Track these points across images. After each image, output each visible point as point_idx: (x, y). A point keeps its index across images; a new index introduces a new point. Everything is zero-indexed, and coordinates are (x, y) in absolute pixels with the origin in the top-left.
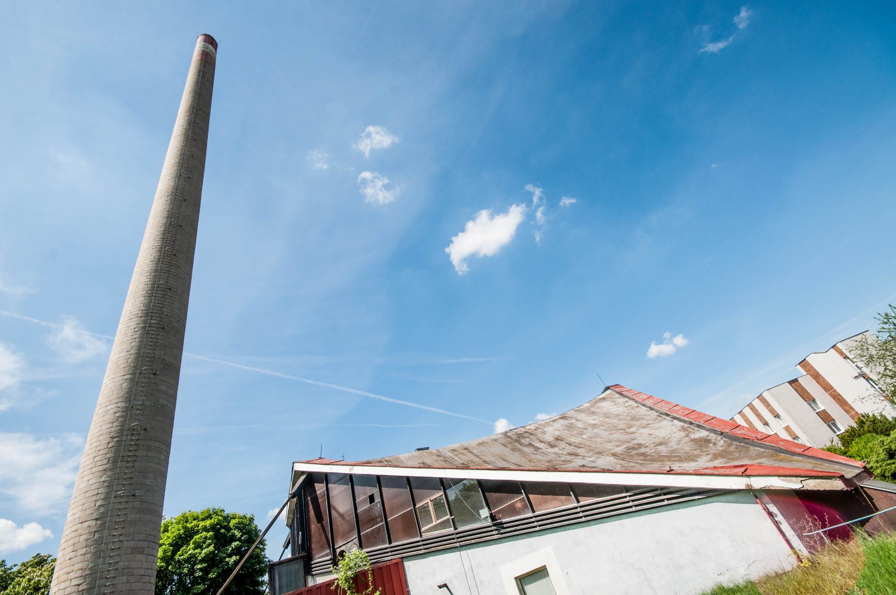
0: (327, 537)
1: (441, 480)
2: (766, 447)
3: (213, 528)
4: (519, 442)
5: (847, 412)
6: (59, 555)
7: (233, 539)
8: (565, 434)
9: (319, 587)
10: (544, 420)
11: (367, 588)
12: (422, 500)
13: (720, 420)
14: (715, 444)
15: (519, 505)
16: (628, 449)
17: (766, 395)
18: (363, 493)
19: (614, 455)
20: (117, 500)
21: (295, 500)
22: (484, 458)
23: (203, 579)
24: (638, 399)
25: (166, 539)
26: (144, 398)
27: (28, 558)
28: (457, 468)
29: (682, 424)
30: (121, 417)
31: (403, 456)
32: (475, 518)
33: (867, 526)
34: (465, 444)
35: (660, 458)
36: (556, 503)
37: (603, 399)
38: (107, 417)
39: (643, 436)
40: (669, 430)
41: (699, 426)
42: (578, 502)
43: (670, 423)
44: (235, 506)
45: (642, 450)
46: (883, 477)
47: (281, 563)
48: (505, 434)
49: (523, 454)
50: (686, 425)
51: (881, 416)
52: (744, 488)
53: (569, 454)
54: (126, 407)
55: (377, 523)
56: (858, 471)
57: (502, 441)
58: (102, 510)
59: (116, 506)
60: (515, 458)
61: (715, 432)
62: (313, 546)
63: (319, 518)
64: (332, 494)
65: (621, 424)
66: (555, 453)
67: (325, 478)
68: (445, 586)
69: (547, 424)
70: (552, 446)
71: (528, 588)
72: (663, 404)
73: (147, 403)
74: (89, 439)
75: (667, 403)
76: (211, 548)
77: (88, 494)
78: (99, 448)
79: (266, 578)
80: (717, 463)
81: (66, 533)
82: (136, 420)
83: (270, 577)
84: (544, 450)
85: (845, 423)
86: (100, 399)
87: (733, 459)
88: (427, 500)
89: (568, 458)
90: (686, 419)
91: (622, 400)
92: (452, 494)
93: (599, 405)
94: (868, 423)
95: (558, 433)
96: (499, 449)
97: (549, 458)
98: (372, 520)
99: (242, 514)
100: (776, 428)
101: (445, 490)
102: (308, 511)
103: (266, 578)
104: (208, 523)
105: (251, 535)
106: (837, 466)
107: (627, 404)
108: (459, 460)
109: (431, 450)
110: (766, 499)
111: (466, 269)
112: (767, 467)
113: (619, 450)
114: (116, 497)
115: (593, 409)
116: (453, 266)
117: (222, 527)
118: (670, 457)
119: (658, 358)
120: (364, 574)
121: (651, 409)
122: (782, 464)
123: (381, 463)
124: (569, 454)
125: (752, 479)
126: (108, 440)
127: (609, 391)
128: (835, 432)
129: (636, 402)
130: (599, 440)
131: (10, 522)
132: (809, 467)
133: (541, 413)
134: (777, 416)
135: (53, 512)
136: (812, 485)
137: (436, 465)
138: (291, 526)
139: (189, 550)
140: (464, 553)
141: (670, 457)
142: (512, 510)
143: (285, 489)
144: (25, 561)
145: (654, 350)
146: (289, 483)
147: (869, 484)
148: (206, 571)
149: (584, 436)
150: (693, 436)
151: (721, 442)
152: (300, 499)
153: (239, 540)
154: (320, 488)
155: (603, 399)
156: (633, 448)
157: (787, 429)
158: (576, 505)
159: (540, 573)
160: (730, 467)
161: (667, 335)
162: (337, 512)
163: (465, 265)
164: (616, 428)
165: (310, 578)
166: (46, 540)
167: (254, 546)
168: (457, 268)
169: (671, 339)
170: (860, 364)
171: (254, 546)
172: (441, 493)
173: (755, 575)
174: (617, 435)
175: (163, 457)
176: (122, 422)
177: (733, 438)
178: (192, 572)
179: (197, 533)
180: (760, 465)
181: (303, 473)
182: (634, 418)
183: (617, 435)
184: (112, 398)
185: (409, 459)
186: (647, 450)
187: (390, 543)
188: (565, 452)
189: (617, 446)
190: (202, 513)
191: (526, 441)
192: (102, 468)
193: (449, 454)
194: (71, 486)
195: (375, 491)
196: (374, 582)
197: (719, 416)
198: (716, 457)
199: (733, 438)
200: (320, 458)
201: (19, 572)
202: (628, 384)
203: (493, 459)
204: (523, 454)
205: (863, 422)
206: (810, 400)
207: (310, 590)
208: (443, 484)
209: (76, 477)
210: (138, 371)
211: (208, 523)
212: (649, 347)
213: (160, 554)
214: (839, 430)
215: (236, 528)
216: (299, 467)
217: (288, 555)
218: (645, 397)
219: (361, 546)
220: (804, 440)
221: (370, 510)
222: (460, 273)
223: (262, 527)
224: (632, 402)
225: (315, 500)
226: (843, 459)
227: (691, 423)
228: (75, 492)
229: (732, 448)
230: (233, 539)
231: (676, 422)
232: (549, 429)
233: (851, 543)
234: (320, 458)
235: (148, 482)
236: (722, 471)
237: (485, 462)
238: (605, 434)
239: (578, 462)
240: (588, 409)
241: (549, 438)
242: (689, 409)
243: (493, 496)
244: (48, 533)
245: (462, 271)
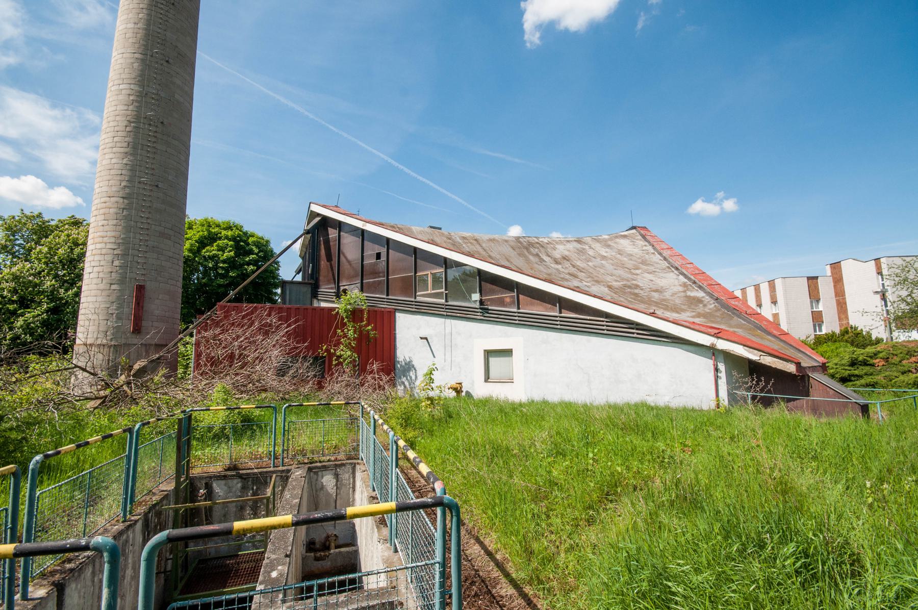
0: (333, 275)
1: (445, 259)
2: (749, 322)
3: (233, 239)
4: (527, 249)
5: (840, 319)
6: (92, 220)
7: (251, 252)
8: (573, 256)
9: (323, 309)
10: (558, 239)
11: (362, 321)
12: (423, 271)
13: (724, 289)
14: (705, 306)
15: (508, 300)
16: (625, 286)
17: (779, 284)
18: (371, 249)
19: (610, 287)
20: (142, 186)
21: (309, 236)
22: (491, 254)
23: (223, 276)
24: (658, 247)
25: (193, 235)
26: (158, 87)
27: (65, 217)
28: (463, 253)
29: (686, 280)
30: (137, 101)
31: (415, 229)
32: (468, 299)
33: (790, 404)
34: (477, 235)
35: (649, 302)
36: (541, 308)
37: (625, 236)
38: (121, 97)
39: (644, 280)
40: (671, 282)
41: (700, 287)
42: (560, 312)
43: (675, 277)
44: (256, 225)
45: (636, 291)
46: (832, 376)
47: (292, 283)
48: (517, 239)
49: (528, 261)
50: (689, 283)
51: (868, 333)
52: (708, 345)
53: (569, 274)
54: (140, 92)
55: (379, 277)
56: (816, 364)
57: (512, 244)
58: (127, 190)
59: (141, 191)
60: (520, 262)
61: (711, 296)
62: (321, 278)
63: (329, 258)
64: (343, 241)
65: (630, 264)
66: (557, 269)
67: (339, 225)
68: (426, 339)
69: (560, 242)
70: (557, 262)
71: (492, 360)
72: (679, 258)
73: (163, 94)
74: (105, 116)
75: (683, 258)
76: (232, 254)
77: (112, 172)
78: (116, 129)
79: (279, 291)
80: (697, 320)
81: (96, 202)
82: (152, 110)
83: (282, 290)
84: (548, 264)
85: (830, 326)
86: (111, 74)
87: (713, 322)
88: (429, 272)
89: (568, 277)
90: (692, 277)
91: (643, 243)
92: (453, 273)
93: (617, 240)
94: (850, 335)
95: (567, 253)
96: (507, 250)
97: (550, 271)
98: (375, 273)
99: (260, 235)
100: (767, 311)
101: (446, 268)
102: (320, 250)
103: (279, 291)
104: (230, 233)
105: (266, 254)
106: (800, 355)
107: (645, 248)
108: (466, 248)
109: (443, 231)
110: (721, 358)
111: (537, 41)
112: (739, 336)
113: (615, 284)
114: (140, 182)
115: (609, 243)
116: (521, 31)
117: (241, 240)
118: (657, 304)
119: (698, 216)
120: (362, 311)
121: (665, 259)
122: (754, 339)
123: (393, 228)
124: (569, 274)
125: (720, 341)
126: (125, 123)
127: (634, 231)
128: (815, 331)
129: (654, 248)
130: (602, 271)
131: (39, 181)
132: (776, 347)
133: (556, 231)
134: (774, 302)
135: (81, 183)
136: (768, 361)
137: (445, 245)
138: (303, 257)
139: (210, 250)
140: (448, 321)
141: (657, 304)
142: (501, 302)
143: (302, 225)
144: (62, 219)
145: (699, 206)
146: (304, 220)
147: (816, 376)
148: (227, 270)
149: (590, 264)
150: (689, 293)
151: (712, 305)
152: (313, 237)
153: (257, 254)
154: (333, 233)
155: (625, 236)
156: (629, 287)
157: (776, 316)
158: (557, 314)
159: (508, 353)
160: (707, 326)
161: (720, 195)
162: (346, 257)
163: (538, 35)
164: (623, 266)
165: (315, 301)
166: (79, 206)
167: (269, 263)
168: (526, 37)
169: (722, 200)
170: (887, 283)
171: (269, 263)
172: (443, 270)
173: (676, 403)
174: (620, 272)
175: (183, 158)
176: (137, 107)
177: (724, 306)
178: (215, 268)
179: (220, 238)
180: (734, 333)
181: (318, 215)
182: (644, 262)
183: (620, 272)
184: (123, 76)
185: (421, 232)
186: (641, 292)
187: (388, 295)
188: (566, 271)
189: (616, 281)
190: (224, 223)
191: (536, 251)
192: (122, 150)
193: (458, 239)
194: (94, 163)
195: (383, 251)
196: (368, 319)
197: (724, 284)
198: (699, 315)
199: (724, 306)
200: (337, 206)
201: (57, 226)
202: (654, 230)
203: (498, 257)
204: (528, 261)
205: (847, 332)
206: (814, 296)
207: (315, 309)
208: (446, 263)
209: (98, 156)
210: (149, 53)
211: (230, 233)
212: (694, 202)
213: (187, 245)
214: (820, 330)
215: (254, 245)
216: (316, 208)
217: (299, 278)
218: (666, 247)
219: (362, 290)
220: (784, 326)
221: (375, 264)
222: (528, 45)
223: (277, 251)
224: (650, 248)
225: (327, 242)
226: (809, 352)
227: (694, 283)
228: (99, 168)
229: (718, 314)
230: (251, 252)
231: (681, 277)
232: (560, 247)
233: (769, 410)
234: (337, 206)
235: (170, 178)
236: (697, 327)
237: (490, 256)
238: (610, 268)
239: (576, 283)
240: (605, 240)
241: (557, 255)
242: (699, 270)
243: (487, 286)
244: (79, 200)
245: (531, 43)
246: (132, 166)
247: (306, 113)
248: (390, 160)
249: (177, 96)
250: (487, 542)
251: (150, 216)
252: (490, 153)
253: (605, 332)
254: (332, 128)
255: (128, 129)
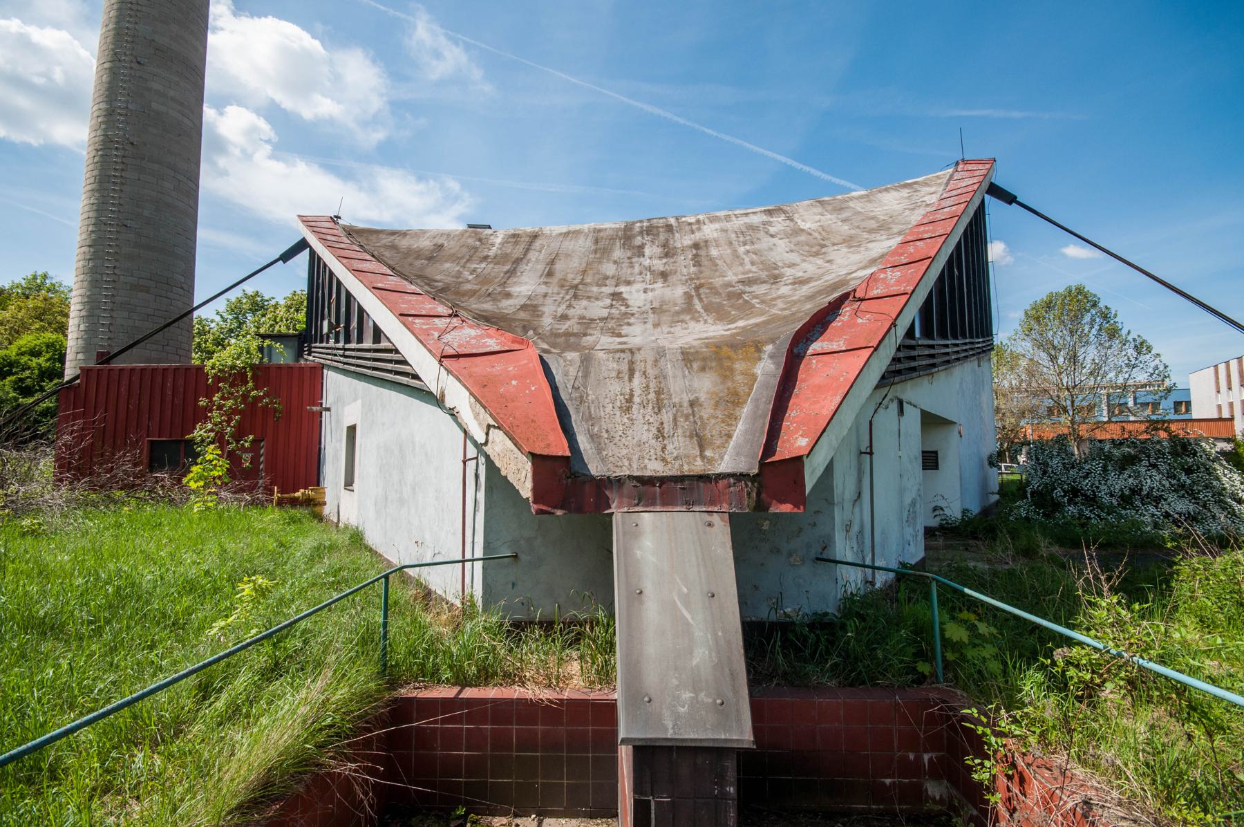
246: (98, 205)
247: (676, 118)
248: (790, 162)
249: (154, 105)
250: (381, 620)
251: (117, 264)
252: (965, 113)
253: (340, 365)
254: (710, 131)
255: (96, 159)
